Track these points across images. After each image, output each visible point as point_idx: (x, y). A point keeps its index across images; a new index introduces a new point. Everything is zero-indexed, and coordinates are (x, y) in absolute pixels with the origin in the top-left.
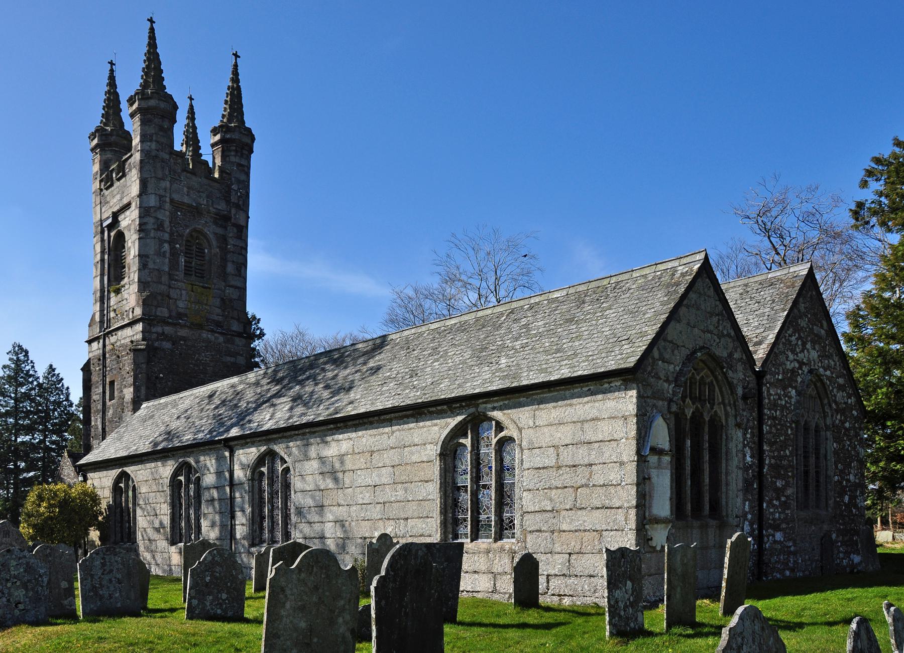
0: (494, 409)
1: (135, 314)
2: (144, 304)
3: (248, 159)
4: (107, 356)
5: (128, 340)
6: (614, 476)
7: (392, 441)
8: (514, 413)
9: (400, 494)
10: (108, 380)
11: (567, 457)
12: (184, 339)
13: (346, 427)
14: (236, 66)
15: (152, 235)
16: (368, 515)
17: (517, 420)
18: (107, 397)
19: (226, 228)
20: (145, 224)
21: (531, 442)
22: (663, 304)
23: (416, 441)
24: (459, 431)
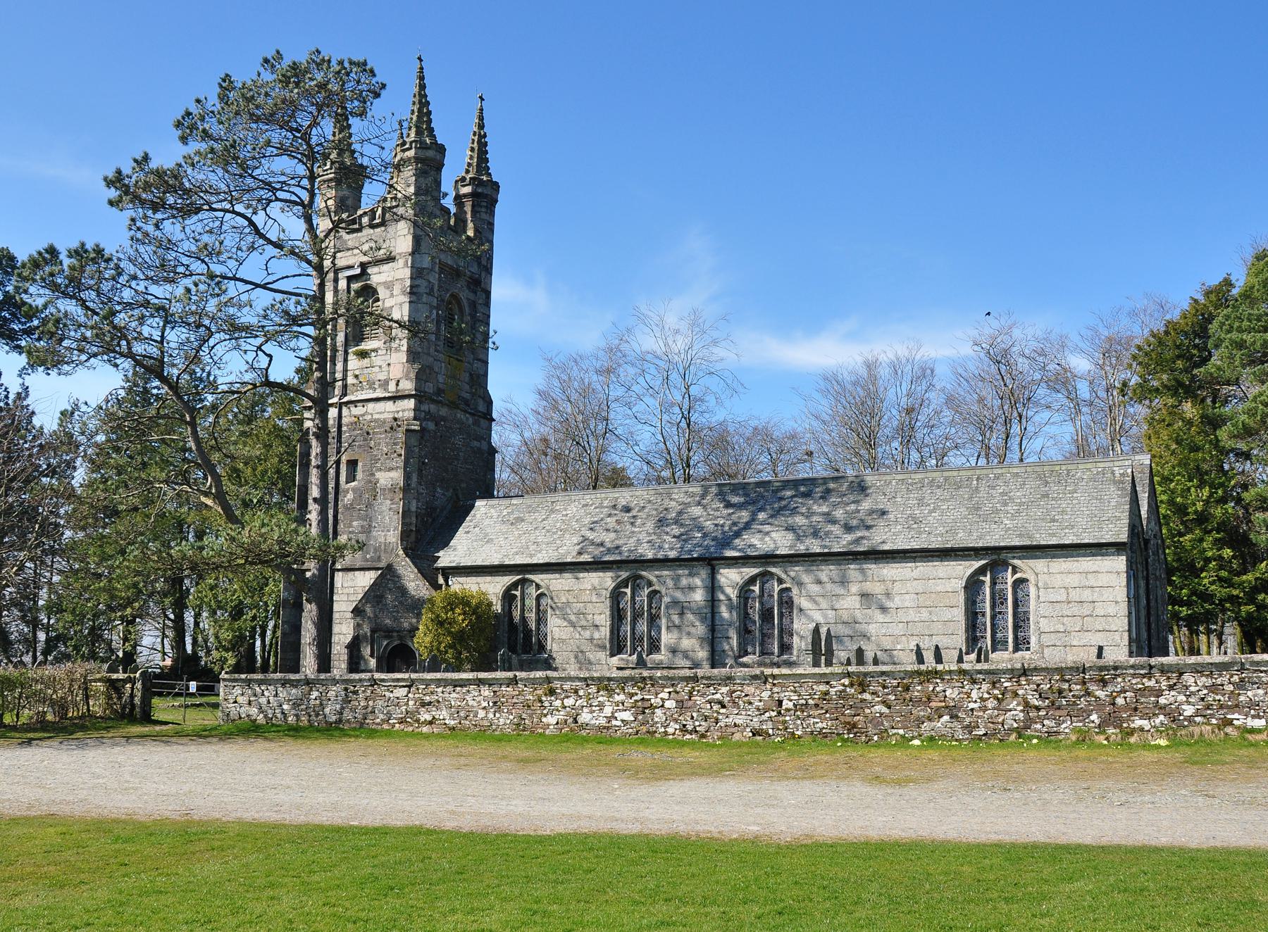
0: (1014, 558)
1: (401, 386)
2: (418, 378)
3: (492, 214)
4: (344, 428)
5: (391, 416)
6: (1112, 610)
7: (916, 573)
8: (1031, 562)
9: (925, 614)
10: (344, 459)
11: (1075, 595)
12: (444, 419)
13: (906, 558)
14: (481, 110)
15: (424, 300)
16: (890, 631)
17: (1031, 568)
18: (343, 478)
19: (475, 293)
20: (417, 286)
21: (1046, 583)
22: (1119, 504)
23: (941, 575)
24: (981, 571)
